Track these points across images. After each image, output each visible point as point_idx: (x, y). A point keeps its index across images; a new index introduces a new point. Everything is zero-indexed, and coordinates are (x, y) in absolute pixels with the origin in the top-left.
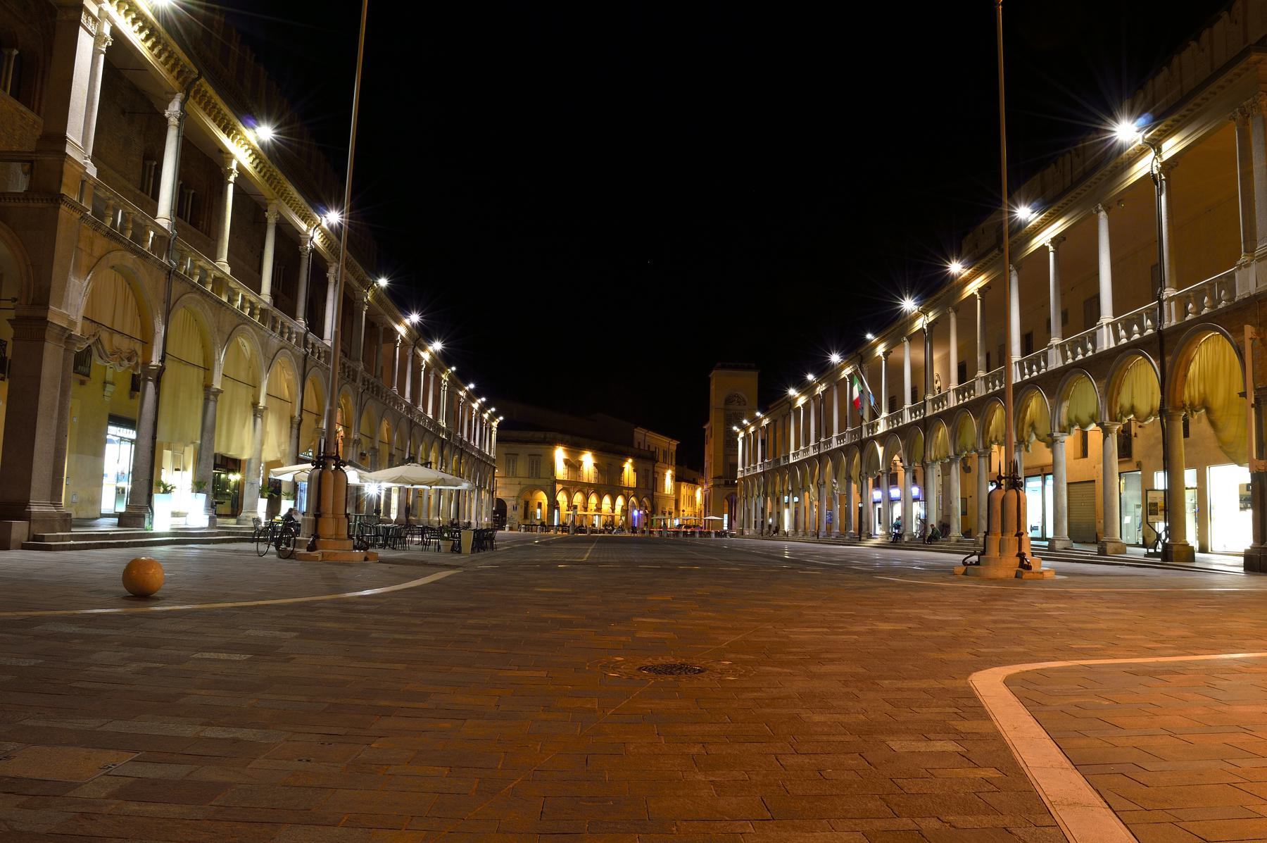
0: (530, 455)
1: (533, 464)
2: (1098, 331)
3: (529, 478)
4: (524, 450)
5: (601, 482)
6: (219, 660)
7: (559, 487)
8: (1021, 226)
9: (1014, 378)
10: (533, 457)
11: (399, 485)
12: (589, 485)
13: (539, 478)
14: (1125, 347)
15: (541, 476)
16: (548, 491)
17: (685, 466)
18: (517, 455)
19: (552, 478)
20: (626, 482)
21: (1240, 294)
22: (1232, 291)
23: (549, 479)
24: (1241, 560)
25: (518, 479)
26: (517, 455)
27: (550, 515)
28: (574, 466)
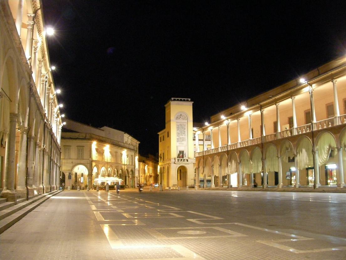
0: (78, 146)
1: (79, 151)
2: (335, 119)
3: (77, 159)
4: (74, 144)
5: (113, 162)
6: (135, 184)
7: (94, 164)
8: (300, 84)
9: (337, 123)
10: (79, 147)
11: (327, 186)
12: (107, 163)
13: (83, 159)
14: (321, 130)
15: (84, 158)
16: (89, 167)
17: (51, 31)
18: (70, 146)
19: (90, 160)
20: (106, 159)
21: (335, 125)
22: (332, 123)
23: (89, 159)
24: (258, 187)
25: (71, 160)
26: (70, 146)
27: (90, 180)
28: (100, 152)
